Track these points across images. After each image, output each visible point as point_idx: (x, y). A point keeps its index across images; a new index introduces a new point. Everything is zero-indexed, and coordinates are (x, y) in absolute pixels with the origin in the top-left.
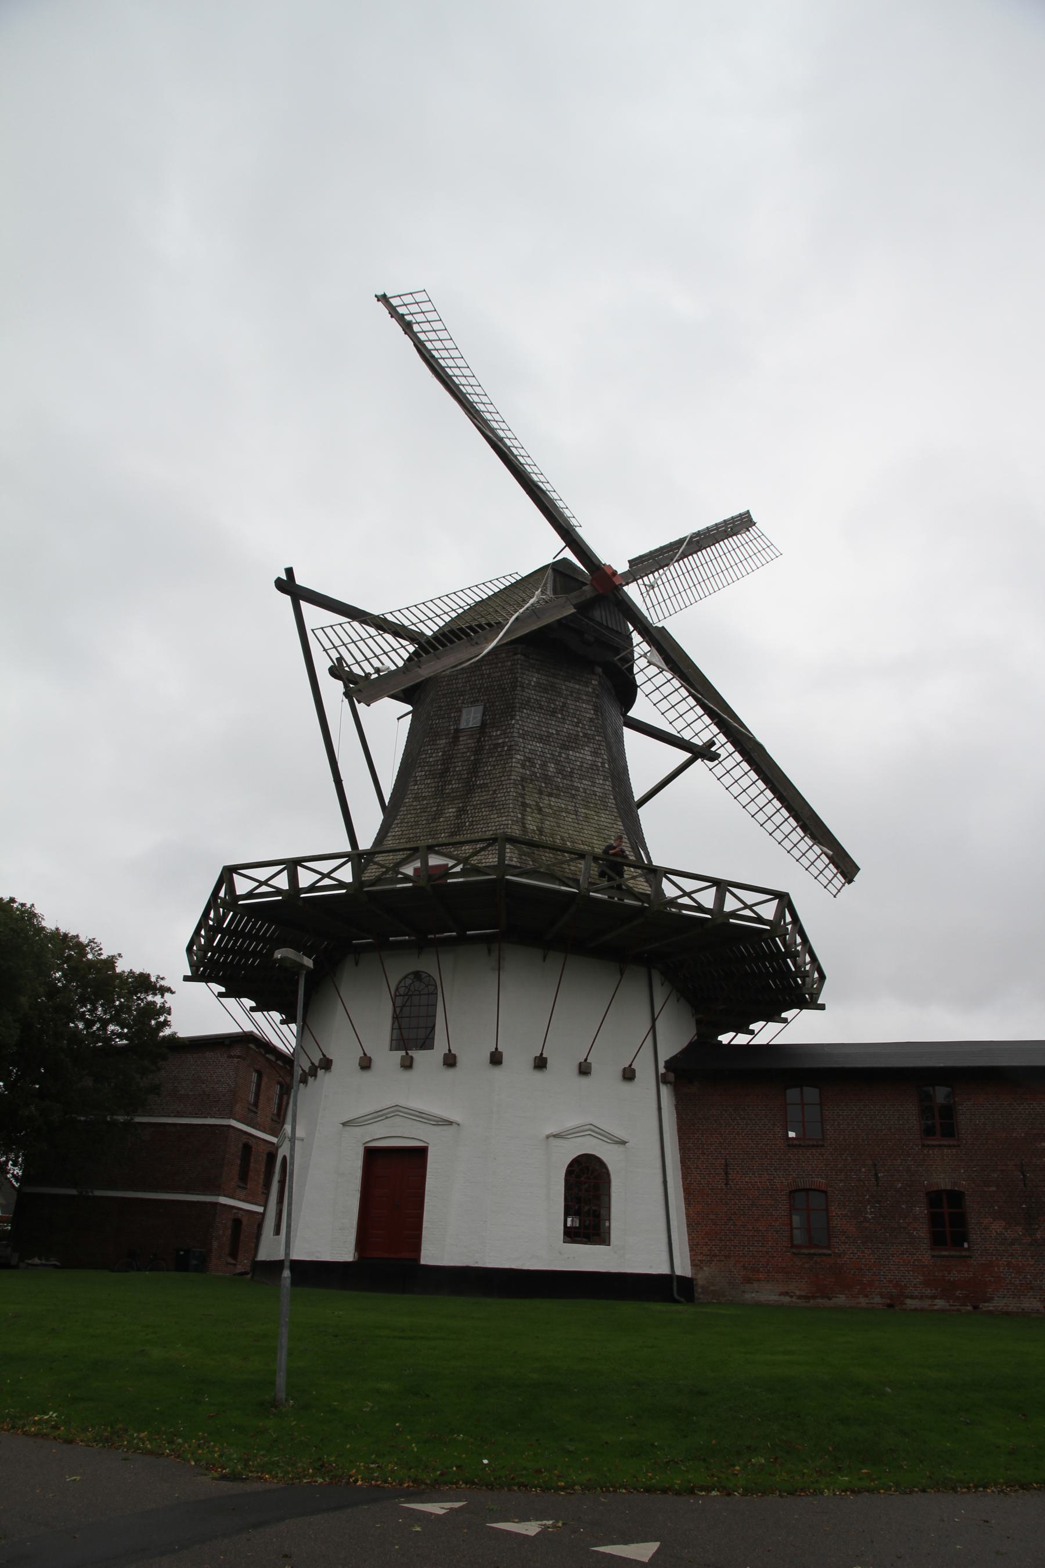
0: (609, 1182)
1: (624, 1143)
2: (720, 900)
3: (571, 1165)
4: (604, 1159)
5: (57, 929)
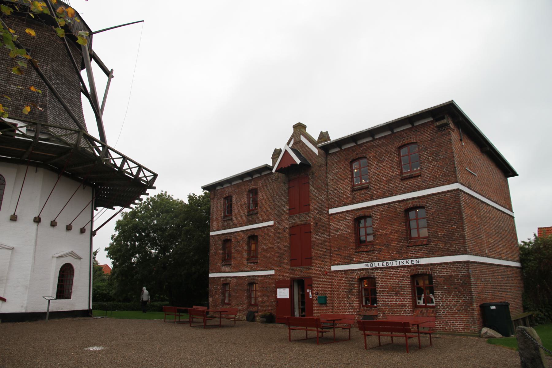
0: (73, 274)
1: (80, 258)
2: (138, 172)
3: (62, 268)
4: (72, 264)
5: (106, 249)
